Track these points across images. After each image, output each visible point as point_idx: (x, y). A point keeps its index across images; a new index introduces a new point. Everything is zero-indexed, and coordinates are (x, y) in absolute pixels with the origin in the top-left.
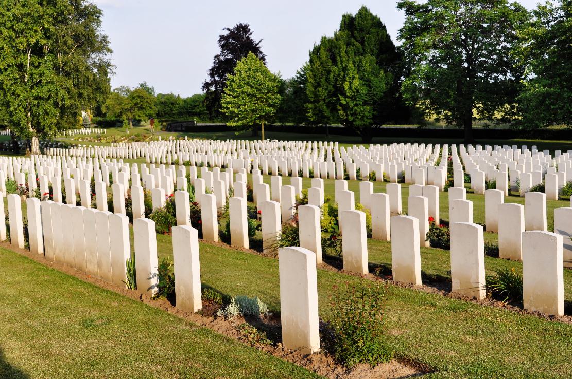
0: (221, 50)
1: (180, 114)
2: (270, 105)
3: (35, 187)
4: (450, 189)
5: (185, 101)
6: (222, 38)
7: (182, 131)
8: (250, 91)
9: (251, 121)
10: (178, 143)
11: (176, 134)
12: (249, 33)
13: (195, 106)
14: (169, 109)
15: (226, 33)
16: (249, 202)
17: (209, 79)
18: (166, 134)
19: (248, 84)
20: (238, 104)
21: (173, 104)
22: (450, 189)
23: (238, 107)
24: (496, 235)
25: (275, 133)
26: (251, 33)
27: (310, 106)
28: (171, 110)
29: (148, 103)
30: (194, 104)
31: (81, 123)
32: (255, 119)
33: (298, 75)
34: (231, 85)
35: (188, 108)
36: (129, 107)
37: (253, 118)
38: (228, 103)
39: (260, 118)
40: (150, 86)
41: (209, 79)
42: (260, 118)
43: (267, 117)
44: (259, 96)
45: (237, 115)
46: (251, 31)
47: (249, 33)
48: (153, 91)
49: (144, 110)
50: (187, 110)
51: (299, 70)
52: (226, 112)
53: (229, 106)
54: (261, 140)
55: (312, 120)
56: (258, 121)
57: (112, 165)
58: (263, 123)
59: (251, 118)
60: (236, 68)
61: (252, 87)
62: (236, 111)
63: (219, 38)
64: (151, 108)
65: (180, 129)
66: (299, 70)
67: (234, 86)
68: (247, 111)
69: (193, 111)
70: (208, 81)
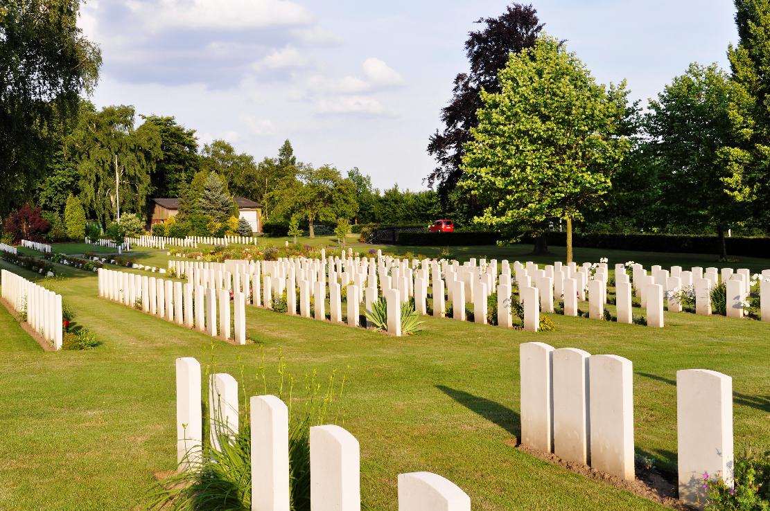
0: (470, 65)
1: (407, 218)
2: (595, 168)
3: (376, 299)
4: (500, 276)
5: (416, 197)
6: (476, 38)
7: (394, 243)
8: (539, 127)
9: (539, 211)
10: (332, 264)
11: (384, 247)
12: (535, 28)
13: (431, 205)
14: (390, 210)
15: (482, 28)
16: (516, 411)
17: (442, 128)
18: (366, 248)
19: (535, 109)
20: (505, 164)
21: (396, 202)
22: (500, 276)
23: (506, 174)
24: (582, 310)
25: (589, 248)
26: (540, 28)
27: (736, 152)
28: (395, 212)
29: (343, 193)
30: (429, 201)
31: (235, 227)
32: (550, 207)
33: (653, 112)
34: (488, 117)
35: (420, 208)
36: (307, 199)
37: (546, 202)
38: (482, 163)
39: (563, 203)
40: (364, 176)
41: (442, 128)
42: (563, 203)
43: (581, 199)
44: (563, 142)
45: (504, 192)
46: (540, 23)
47: (535, 28)
48: (368, 183)
49: (333, 205)
50: (418, 210)
51: (657, 99)
52: (473, 189)
53: (483, 172)
54: (565, 263)
55: (739, 198)
56: (557, 213)
57: (544, 276)
58: (569, 216)
59: (540, 201)
60: (504, 71)
61: (545, 119)
62: (499, 182)
63: (469, 38)
64: (346, 201)
65: (391, 240)
66: (657, 99)
67: (496, 116)
68: (530, 182)
69: (428, 212)
70: (441, 134)
